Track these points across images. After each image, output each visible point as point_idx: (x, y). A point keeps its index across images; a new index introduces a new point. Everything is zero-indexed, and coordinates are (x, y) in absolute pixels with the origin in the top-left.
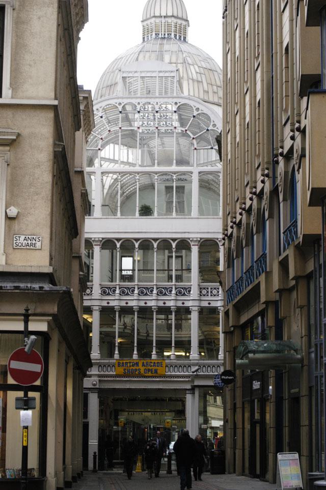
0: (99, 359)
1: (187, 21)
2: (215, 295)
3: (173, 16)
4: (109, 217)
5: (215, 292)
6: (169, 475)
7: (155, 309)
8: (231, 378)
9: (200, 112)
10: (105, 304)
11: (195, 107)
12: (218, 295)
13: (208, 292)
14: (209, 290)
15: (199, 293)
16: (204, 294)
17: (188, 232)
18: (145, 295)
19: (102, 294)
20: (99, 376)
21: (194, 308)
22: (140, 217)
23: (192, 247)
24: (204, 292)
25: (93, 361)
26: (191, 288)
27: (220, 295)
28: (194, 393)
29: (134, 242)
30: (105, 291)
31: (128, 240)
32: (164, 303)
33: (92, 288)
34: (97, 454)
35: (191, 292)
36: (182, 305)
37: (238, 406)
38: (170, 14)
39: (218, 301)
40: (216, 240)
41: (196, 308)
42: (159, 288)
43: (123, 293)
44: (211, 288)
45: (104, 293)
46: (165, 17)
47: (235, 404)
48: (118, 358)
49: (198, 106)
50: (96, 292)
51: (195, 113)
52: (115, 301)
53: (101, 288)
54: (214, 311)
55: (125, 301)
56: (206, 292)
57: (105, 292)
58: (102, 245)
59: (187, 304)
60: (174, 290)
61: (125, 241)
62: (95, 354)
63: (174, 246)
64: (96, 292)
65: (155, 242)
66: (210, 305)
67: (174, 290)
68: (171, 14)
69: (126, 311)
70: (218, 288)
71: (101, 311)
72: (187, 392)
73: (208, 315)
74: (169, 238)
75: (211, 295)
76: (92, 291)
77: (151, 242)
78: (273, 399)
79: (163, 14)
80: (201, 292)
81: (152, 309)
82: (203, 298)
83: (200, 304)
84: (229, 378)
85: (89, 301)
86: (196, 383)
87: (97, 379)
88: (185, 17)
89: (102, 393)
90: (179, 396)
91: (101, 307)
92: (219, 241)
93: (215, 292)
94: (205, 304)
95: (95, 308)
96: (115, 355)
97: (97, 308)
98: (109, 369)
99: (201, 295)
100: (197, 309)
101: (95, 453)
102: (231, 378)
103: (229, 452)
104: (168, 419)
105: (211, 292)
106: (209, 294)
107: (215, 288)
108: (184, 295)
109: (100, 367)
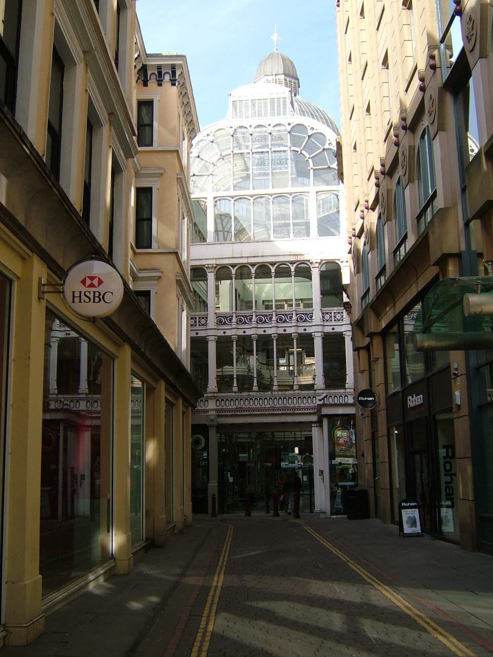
0: (217, 393)
2: (339, 320)
4: (195, 244)
6: (247, 518)
8: (371, 399)
10: (221, 333)
12: (342, 320)
13: (331, 317)
14: (198, 320)
16: (327, 319)
18: (243, 323)
19: (217, 324)
20: (216, 410)
21: (317, 334)
22: (296, 238)
23: (208, 274)
24: (327, 317)
25: (50, 396)
26: (313, 313)
27: (344, 320)
28: (321, 426)
29: (251, 267)
31: (243, 266)
33: (207, 318)
34: (216, 496)
35: (313, 318)
36: (224, 335)
39: (344, 326)
40: (337, 261)
41: (319, 334)
42: (279, 315)
44: (199, 318)
45: (220, 322)
48: (257, 390)
50: (212, 321)
51: (310, 133)
52: (233, 331)
54: (340, 337)
56: (329, 317)
57: (221, 322)
58: (216, 272)
59: (310, 330)
60: (294, 315)
61: (222, 267)
62: (212, 385)
63: (293, 270)
64: (212, 321)
65: (273, 267)
66: (334, 331)
67: (294, 315)
69: (244, 343)
70: (342, 313)
71: (323, 339)
72: (69, 430)
73: (333, 342)
74: (248, 263)
75: (335, 320)
76: (207, 321)
78: (465, 411)
82: (326, 324)
83: (323, 329)
84: (368, 399)
86: (325, 411)
87: (214, 413)
89: (220, 428)
92: (206, 268)
94: (328, 330)
95: (210, 338)
96: (254, 387)
97: (213, 338)
98: (256, 401)
99: (324, 321)
100: (214, 339)
101: (214, 495)
102: (371, 399)
104: (205, 456)
105: (199, 322)
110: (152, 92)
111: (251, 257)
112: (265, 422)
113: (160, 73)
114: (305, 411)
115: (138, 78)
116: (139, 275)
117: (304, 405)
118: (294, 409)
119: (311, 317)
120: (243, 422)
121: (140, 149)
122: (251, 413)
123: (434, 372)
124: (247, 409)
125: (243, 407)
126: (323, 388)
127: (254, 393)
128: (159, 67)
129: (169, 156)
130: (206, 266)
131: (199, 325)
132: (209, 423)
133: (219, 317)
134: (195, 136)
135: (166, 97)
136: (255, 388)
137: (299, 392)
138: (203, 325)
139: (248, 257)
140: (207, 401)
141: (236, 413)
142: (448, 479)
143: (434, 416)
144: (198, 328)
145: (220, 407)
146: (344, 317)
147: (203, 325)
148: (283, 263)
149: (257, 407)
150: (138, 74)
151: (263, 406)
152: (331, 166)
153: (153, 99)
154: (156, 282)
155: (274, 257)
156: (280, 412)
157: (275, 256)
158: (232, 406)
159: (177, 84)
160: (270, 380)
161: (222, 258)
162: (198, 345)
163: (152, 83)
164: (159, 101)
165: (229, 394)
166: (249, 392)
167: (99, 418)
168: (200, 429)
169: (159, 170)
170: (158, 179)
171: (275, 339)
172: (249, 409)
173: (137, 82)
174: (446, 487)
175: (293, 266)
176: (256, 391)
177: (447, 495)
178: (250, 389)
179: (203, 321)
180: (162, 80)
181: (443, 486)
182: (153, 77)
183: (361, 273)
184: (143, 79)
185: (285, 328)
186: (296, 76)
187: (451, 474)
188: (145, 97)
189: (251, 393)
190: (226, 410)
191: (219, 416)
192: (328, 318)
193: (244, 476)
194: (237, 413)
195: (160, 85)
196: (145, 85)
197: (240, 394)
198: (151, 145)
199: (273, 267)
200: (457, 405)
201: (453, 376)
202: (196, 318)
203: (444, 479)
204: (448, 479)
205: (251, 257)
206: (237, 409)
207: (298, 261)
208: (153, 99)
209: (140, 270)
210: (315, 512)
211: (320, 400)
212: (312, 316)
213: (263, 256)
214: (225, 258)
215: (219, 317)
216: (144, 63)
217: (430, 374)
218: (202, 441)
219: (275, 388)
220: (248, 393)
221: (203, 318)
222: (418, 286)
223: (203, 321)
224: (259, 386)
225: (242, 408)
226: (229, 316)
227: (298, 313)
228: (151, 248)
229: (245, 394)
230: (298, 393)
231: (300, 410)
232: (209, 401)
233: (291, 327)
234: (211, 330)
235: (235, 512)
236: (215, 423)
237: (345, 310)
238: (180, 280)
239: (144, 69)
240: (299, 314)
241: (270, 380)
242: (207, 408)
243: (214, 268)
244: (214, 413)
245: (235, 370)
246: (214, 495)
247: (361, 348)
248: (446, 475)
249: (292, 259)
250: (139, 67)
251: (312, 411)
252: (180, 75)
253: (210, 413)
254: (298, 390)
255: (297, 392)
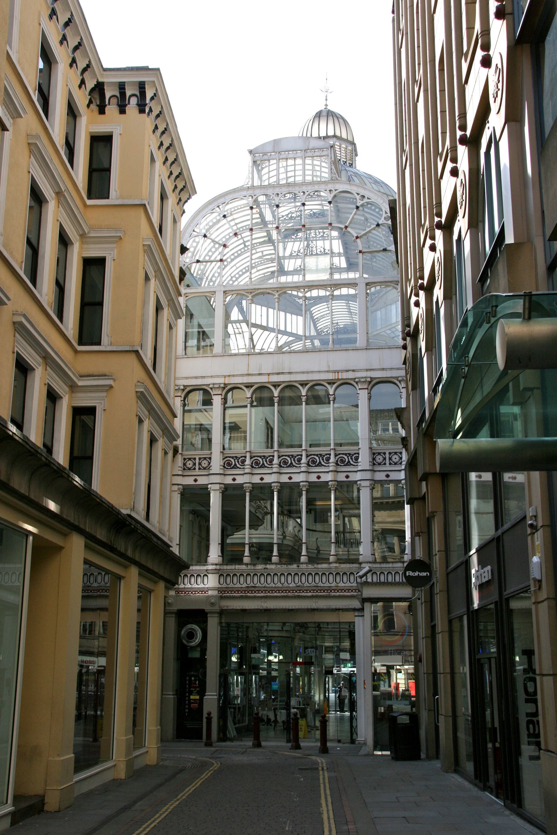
1: (353, 144)
3: (335, 136)
5: (395, 458)
7: (304, 486)
8: (424, 574)
9: (366, 200)
10: (228, 480)
11: (358, 194)
12: (401, 463)
13: (385, 459)
15: (371, 460)
17: (353, 371)
21: (364, 483)
23: (214, 397)
24: (379, 459)
26: (358, 454)
30: (230, 463)
31: (290, 386)
32: (290, 478)
33: (210, 458)
35: (360, 460)
37: (439, 629)
38: (331, 133)
43: (283, 464)
44: (390, 453)
46: (324, 138)
47: (433, 627)
49: (362, 192)
52: (244, 478)
53: (223, 459)
55: (316, 475)
56: (381, 459)
57: (229, 464)
59: (354, 477)
65: (304, 388)
68: (332, 134)
70: (401, 453)
74: (268, 382)
75: (385, 453)
76: (210, 463)
77: (298, 388)
79: (323, 134)
80: (374, 459)
81: (300, 486)
82: (377, 468)
84: (421, 574)
85: (181, 477)
88: (350, 139)
90: (331, 669)
91: (181, 487)
92: (211, 388)
93: (395, 458)
97: (217, 487)
101: (209, 714)
102: (424, 574)
103: (424, 717)
105: (390, 459)
106: (387, 462)
107: (396, 453)
108: (349, 464)
109: (222, 577)
110: (111, 123)
111: (273, 374)
112: (287, 607)
113: (123, 94)
114: (345, 594)
115: (90, 102)
116: (80, 383)
117: (343, 585)
118: (330, 589)
119: (357, 459)
120: (256, 607)
121: (89, 202)
122: (268, 593)
123: (506, 527)
124: (310, 589)
125: (257, 585)
126: (371, 560)
127: (273, 567)
128: (122, 87)
129: (132, 213)
130: (211, 386)
131: (200, 469)
132: (207, 608)
133: (227, 457)
134: (188, 199)
135: (128, 130)
136: (275, 559)
137: (337, 565)
138: (205, 469)
139: (269, 374)
140: (207, 576)
141: (247, 593)
142: (530, 708)
143: (507, 600)
144: (197, 472)
145: (225, 585)
146: (403, 460)
147: (205, 469)
148: (318, 384)
149: (277, 585)
150: (90, 94)
151: (286, 584)
152: (388, 248)
153: (112, 132)
154: (105, 394)
155: (305, 375)
156: (310, 594)
157: (308, 372)
158: (242, 583)
159: (147, 111)
160: (316, 551)
161: (233, 376)
162: (194, 501)
163: (112, 109)
164: (120, 134)
165: (237, 567)
166: (266, 564)
167: (107, 597)
168: (190, 617)
169: (116, 233)
170: (115, 245)
171: (304, 489)
172: (266, 589)
173: (88, 106)
174: (529, 722)
175: (332, 387)
176: (276, 564)
177: (529, 736)
178: (268, 560)
179: (205, 463)
180: (126, 105)
181: (523, 721)
182: (114, 101)
183: (418, 389)
184: (98, 103)
185: (319, 474)
186: (351, 140)
187: (532, 698)
188: (101, 128)
189: (268, 566)
190: (232, 590)
191: (221, 598)
192: (203, 465)
193: (227, 688)
194: (248, 594)
195: (122, 111)
196: (102, 111)
197: (252, 567)
198: (99, 343)
199: (304, 388)
200: (535, 580)
201: (529, 531)
202: (195, 459)
203: (524, 708)
204: (530, 708)
205: (273, 374)
206: (249, 589)
207: (338, 379)
208: (112, 132)
209: (81, 376)
210: (357, 742)
211: (361, 577)
212: (358, 457)
213: (290, 373)
214: (237, 375)
215: (227, 457)
216: (101, 80)
217: (500, 532)
218: (197, 634)
219: (303, 559)
220: (264, 566)
221: (205, 459)
222: (482, 392)
223: (205, 463)
224: (280, 555)
225: (256, 587)
226: (242, 457)
227: (338, 452)
228: (100, 345)
229: (260, 567)
230: (336, 567)
231: (338, 591)
232: (210, 575)
233: (328, 472)
234: (215, 476)
235: (243, 739)
236: (217, 608)
237: (404, 450)
238: (142, 392)
239: (99, 88)
240: (340, 454)
241: (316, 551)
242: (206, 586)
243: (221, 389)
244: (215, 593)
245: (246, 535)
246: (209, 714)
247: (416, 499)
248: (527, 701)
249: (331, 376)
250: (90, 84)
251: (355, 593)
252: (152, 99)
253: (210, 593)
254: (336, 563)
255: (335, 565)
